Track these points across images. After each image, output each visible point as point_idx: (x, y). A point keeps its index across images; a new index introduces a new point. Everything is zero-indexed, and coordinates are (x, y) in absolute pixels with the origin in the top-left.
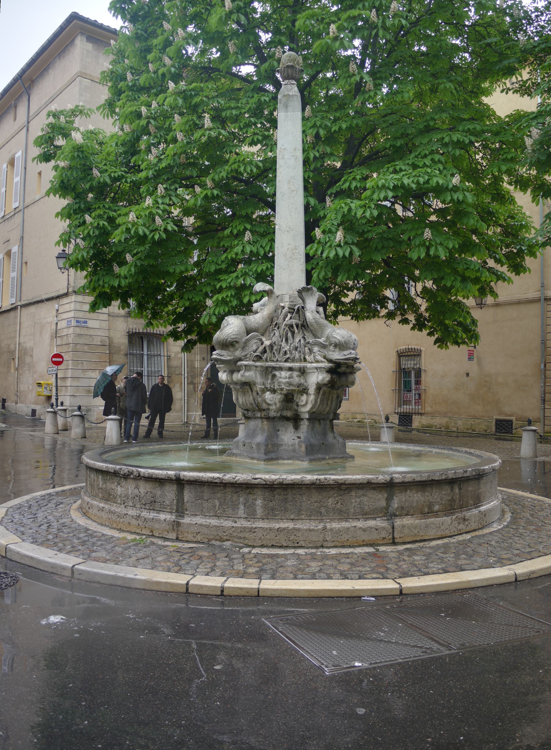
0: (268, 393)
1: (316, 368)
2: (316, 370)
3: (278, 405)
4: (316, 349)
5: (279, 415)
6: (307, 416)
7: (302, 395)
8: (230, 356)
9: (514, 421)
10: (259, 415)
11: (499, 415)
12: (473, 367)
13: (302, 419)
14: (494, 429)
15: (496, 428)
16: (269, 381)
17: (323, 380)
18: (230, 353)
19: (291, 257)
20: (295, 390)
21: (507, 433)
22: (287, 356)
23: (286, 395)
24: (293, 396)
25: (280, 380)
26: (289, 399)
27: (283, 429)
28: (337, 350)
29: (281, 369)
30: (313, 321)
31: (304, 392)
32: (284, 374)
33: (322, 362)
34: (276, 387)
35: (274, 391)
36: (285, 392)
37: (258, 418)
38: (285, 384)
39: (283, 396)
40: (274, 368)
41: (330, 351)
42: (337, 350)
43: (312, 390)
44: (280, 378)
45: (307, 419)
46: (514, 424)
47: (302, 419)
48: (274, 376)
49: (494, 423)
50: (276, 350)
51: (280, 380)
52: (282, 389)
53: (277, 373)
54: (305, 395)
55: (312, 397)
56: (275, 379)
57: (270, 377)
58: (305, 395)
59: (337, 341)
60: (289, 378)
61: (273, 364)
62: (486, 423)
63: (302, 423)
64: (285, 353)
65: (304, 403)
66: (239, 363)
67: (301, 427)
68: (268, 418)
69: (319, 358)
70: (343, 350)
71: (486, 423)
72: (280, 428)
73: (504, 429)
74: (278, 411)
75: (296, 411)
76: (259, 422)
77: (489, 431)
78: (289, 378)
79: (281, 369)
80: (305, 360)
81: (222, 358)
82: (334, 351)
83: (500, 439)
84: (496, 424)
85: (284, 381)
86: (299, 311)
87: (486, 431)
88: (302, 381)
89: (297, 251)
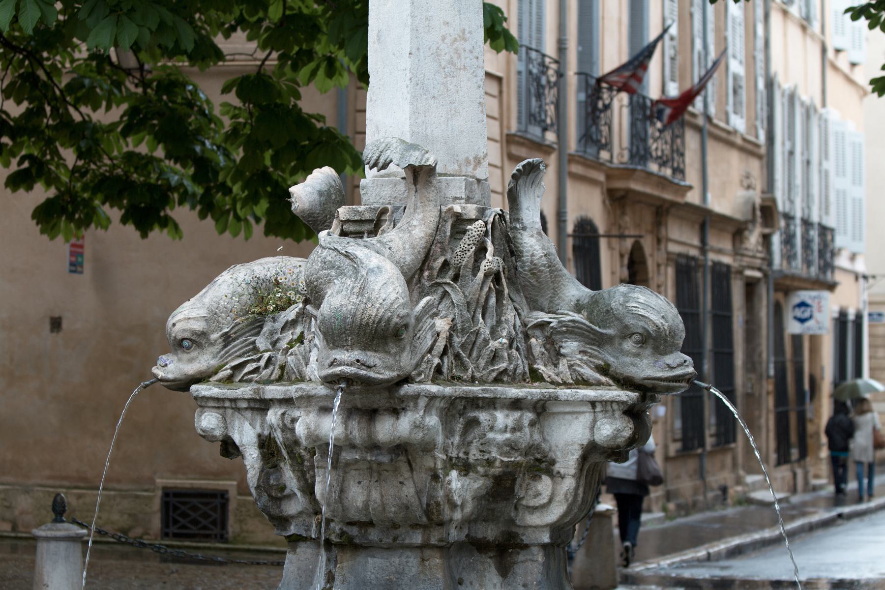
0: (454, 474)
1: (593, 404)
2: (588, 408)
3: (469, 509)
4: (570, 346)
5: (463, 537)
6: (546, 538)
7: (536, 477)
8: (390, 368)
9: (233, 494)
10: (417, 538)
11: (175, 473)
12: (82, 303)
13: (526, 547)
14: (156, 523)
15: (166, 523)
16: (457, 439)
17: (615, 437)
18: (390, 360)
19: (451, 62)
20: (518, 465)
21: (207, 537)
22: (503, 365)
23: (498, 480)
24: (514, 480)
25: (491, 435)
26: (503, 488)
27: (473, 576)
28: (648, 351)
29: (492, 404)
30: (544, 261)
31: (540, 470)
32: (502, 418)
33: (599, 384)
34: (474, 455)
35: (466, 468)
36: (497, 470)
37: (411, 547)
38: (499, 446)
39: (489, 482)
40: (475, 402)
41: (623, 353)
42: (648, 351)
43: (568, 463)
44: (492, 428)
45: (544, 546)
46: (232, 506)
47: (526, 547)
48: (474, 423)
49: (157, 504)
50: (463, 346)
51: (491, 435)
52: (490, 463)
53: (483, 416)
54: (546, 481)
55: (568, 484)
56: (477, 431)
57: (459, 427)
58: (546, 481)
59: (651, 328)
60: (514, 430)
61: (476, 389)
62: (126, 504)
63: (521, 558)
64: (495, 357)
65: (543, 500)
66: (408, 389)
67: (519, 569)
68: (445, 548)
69: (588, 372)
70: (665, 353)
71: (126, 504)
72: (465, 576)
73: (195, 522)
74: (469, 521)
75: (512, 522)
76: (412, 561)
77: (138, 531)
78: (514, 430)
79: (492, 404)
80: (535, 376)
81: (373, 375)
82: (637, 355)
83: (177, 560)
84: (166, 506)
85: (500, 437)
86: (505, 234)
87: (125, 531)
88: (537, 437)
89: (468, 46)
